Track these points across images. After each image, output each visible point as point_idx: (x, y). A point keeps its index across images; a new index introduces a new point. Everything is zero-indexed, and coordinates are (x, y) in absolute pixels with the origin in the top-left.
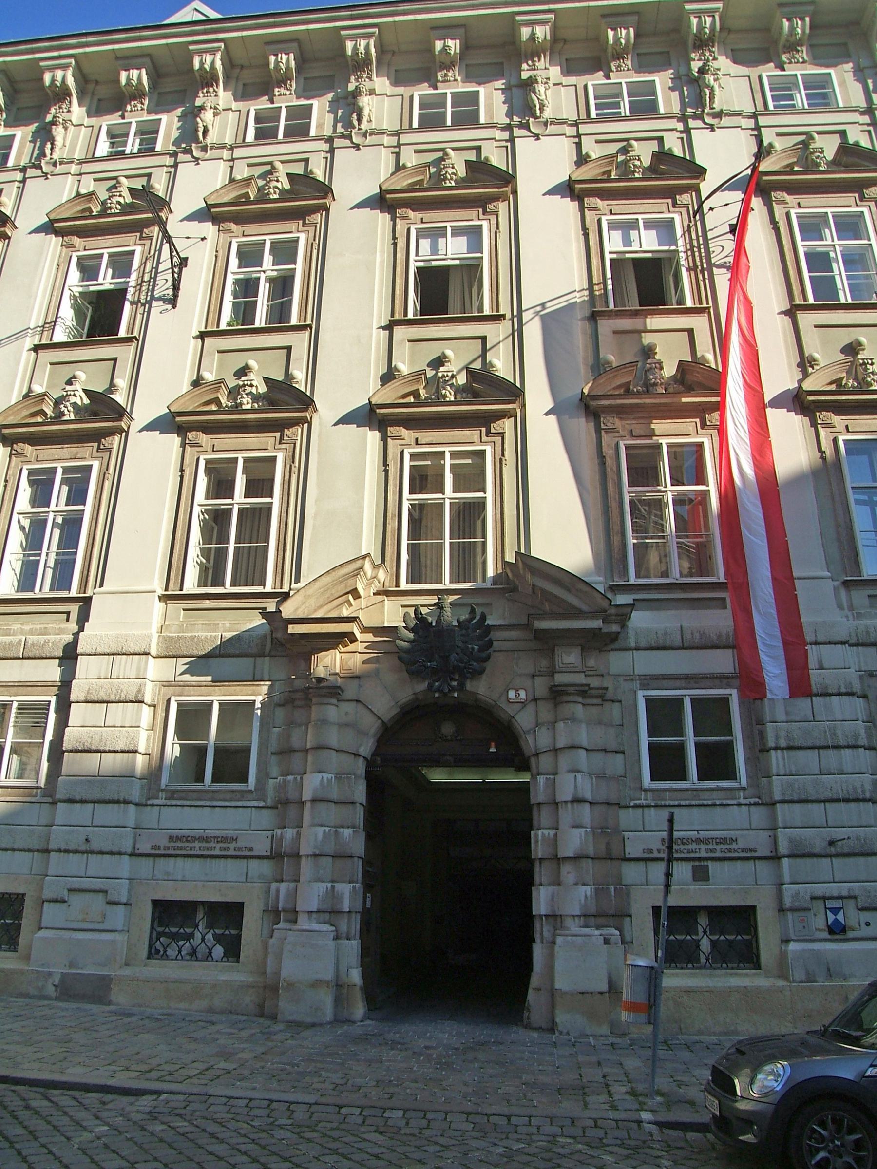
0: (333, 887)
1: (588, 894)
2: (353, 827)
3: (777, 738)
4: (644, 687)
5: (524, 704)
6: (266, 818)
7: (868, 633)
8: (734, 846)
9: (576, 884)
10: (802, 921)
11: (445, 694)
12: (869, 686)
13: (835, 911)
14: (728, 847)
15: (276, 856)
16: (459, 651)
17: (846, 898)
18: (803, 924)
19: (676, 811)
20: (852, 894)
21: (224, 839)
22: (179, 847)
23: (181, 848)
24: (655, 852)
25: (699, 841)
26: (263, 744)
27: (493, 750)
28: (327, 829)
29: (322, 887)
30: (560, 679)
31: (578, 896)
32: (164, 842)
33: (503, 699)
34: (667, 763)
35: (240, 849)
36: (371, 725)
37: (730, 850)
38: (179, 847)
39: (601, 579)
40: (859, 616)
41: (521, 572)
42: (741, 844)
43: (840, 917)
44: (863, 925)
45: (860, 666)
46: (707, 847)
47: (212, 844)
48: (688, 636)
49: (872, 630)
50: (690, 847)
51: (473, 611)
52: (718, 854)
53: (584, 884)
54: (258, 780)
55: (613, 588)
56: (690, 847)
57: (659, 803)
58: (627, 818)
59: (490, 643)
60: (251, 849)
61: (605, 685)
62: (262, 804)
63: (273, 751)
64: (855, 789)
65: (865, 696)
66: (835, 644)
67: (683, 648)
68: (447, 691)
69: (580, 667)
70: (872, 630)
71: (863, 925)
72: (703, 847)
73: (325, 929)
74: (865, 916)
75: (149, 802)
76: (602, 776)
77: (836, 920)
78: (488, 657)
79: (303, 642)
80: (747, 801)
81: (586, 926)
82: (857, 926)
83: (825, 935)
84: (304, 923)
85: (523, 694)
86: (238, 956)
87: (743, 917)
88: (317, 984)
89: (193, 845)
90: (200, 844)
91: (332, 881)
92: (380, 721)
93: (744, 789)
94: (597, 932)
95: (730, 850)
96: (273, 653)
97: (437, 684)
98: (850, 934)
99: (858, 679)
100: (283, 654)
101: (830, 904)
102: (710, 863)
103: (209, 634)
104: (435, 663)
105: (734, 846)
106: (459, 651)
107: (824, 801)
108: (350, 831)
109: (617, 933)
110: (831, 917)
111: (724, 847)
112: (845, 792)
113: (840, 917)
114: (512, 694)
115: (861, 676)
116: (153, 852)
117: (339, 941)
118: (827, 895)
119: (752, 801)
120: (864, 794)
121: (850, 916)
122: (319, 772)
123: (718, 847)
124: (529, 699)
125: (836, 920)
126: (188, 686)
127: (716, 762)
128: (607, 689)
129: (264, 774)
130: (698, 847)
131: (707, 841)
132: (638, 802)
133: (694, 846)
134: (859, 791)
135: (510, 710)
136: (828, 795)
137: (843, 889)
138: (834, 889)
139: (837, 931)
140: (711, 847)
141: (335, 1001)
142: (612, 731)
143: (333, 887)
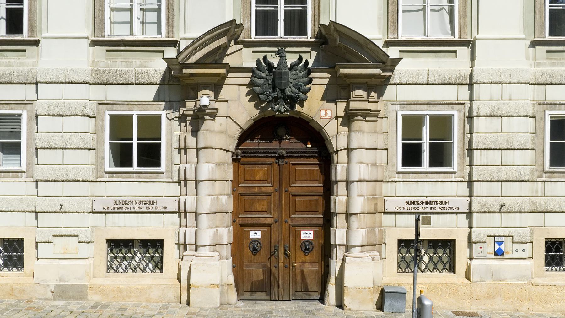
0: (217, 230)
1: (364, 234)
2: (228, 195)
3: (478, 143)
4: (403, 109)
5: (330, 119)
6: (174, 189)
7: (542, 76)
8: (446, 205)
9: (358, 228)
10: (481, 248)
11: (281, 113)
12: (537, 111)
13: (500, 243)
14: (443, 206)
15: (182, 213)
16: (291, 85)
17: (506, 236)
18: (481, 250)
19: (302, 54)
20: (510, 234)
21: (148, 202)
22: (120, 209)
23: (120, 208)
24: (402, 208)
25: (427, 202)
26: (169, 142)
27: (309, 146)
28: (213, 197)
29: (211, 232)
30: (353, 105)
31: (359, 236)
32: (111, 205)
33: (318, 116)
34: (411, 156)
35: (159, 208)
36: (236, 132)
37: (444, 208)
38: (120, 209)
39: (380, 36)
40: (539, 64)
41: (332, 32)
42: (451, 205)
43: (502, 247)
44: (514, 251)
45: (534, 97)
46: (431, 206)
47: (141, 205)
48: (431, 76)
49: (545, 75)
50: (422, 206)
51: (300, 59)
52: (437, 210)
53: (362, 229)
54: (167, 166)
55: (389, 44)
56: (422, 206)
57: (406, 180)
58: (387, 188)
59: (310, 81)
60: (166, 208)
61: (379, 109)
62: (170, 180)
63: (175, 147)
64: (520, 174)
65: (534, 117)
66: (521, 84)
67: (428, 84)
68: (283, 111)
69: (366, 98)
70: (545, 75)
71: (514, 251)
72: (429, 206)
73: (214, 255)
74: (516, 246)
75: (98, 180)
76: (374, 165)
77: (500, 249)
78: (310, 89)
79: (191, 78)
80: (456, 180)
81: (362, 252)
82: (511, 251)
83: (493, 256)
84: (203, 251)
85: (329, 113)
86: (161, 269)
87: (449, 245)
88: (212, 286)
89: (129, 206)
90: (134, 206)
91: (217, 227)
92: (241, 130)
93: (455, 173)
94: (368, 254)
95: (444, 208)
96: (171, 83)
97: (276, 107)
98: (506, 256)
99: (531, 106)
100: (178, 83)
101: (497, 239)
102: (432, 216)
103: (127, 69)
104: (276, 93)
105: (446, 205)
106: (291, 85)
107: (502, 149)
108: (226, 197)
109: (378, 254)
110: (497, 247)
111: (441, 206)
112: (514, 176)
113: (502, 247)
114: (323, 113)
115: (534, 104)
116: (104, 210)
117: (222, 261)
118: (496, 235)
119: (459, 179)
120: (525, 177)
121: (507, 246)
122: (207, 163)
123: (437, 206)
124: (333, 117)
125: (500, 249)
126: (115, 104)
127: (440, 156)
128: (379, 111)
129: (170, 162)
130: (426, 206)
131: (431, 202)
132: (393, 179)
133: (424, 205)
134: (523, 176)
135: (322, 123)
136: (504, 178)
137: (505, 232)
138: (501, 232)
139: (499, 254)
140: (433, 206)
141: (221, 294)
142: (381, 137)
143: (217, 230)
